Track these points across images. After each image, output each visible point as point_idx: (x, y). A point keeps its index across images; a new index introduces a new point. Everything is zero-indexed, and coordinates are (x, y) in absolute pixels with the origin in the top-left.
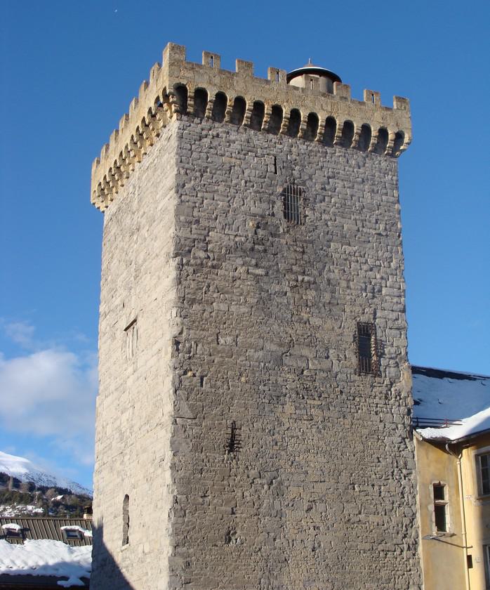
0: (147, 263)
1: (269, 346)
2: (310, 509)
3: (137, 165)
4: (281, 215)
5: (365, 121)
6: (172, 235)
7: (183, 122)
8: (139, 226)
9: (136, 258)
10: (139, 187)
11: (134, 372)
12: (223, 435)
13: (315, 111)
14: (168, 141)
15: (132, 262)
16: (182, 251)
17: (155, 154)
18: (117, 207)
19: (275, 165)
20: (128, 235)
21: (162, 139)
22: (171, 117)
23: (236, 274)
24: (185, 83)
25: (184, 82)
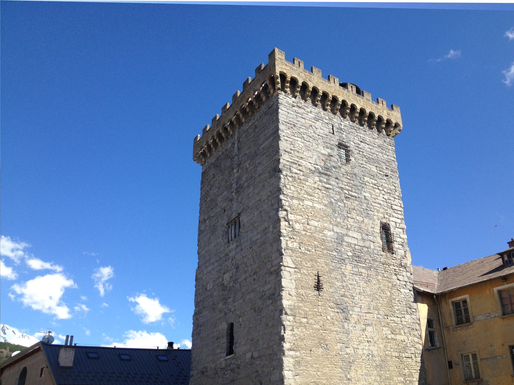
1: (336, 229)
2: (364, 330)
11: (237, 246)
12: (313, 282)
15: (232, 184)
19: (333, 129)
23: (316, 186)
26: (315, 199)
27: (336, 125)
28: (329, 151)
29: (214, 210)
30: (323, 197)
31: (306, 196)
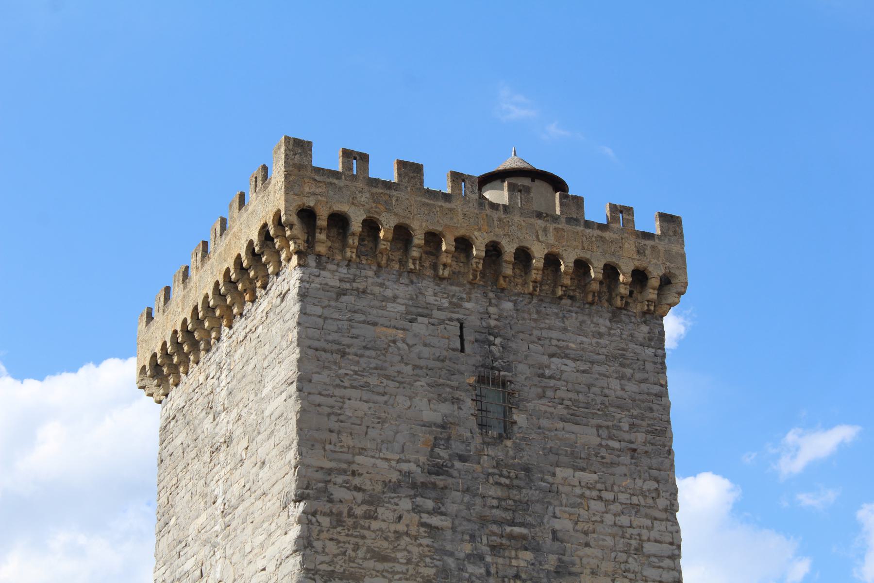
0: (246, 504)
3: (225, 331)
4: (473, 423)
5: (610, 259)
6: (293, 462)
7: (309, 271)
8: (230, 437)
9: (225, 492)
10: (230, 370)
13: (526, 244)
14: (282, 301)
16: (312, 489)
17: (259, 317)
18: (184, 397)
19: (461, 336)
20: (207, 450)
21: (271, 293)
22: (289, 260)
23: (401, 527)
24: (312, 205)
25: (311, 202)
26: (398, 568)
27: (473, 321)
28: (446, 408)
29: (182, 558)
30: (422, 557)
31: (371, 564)
